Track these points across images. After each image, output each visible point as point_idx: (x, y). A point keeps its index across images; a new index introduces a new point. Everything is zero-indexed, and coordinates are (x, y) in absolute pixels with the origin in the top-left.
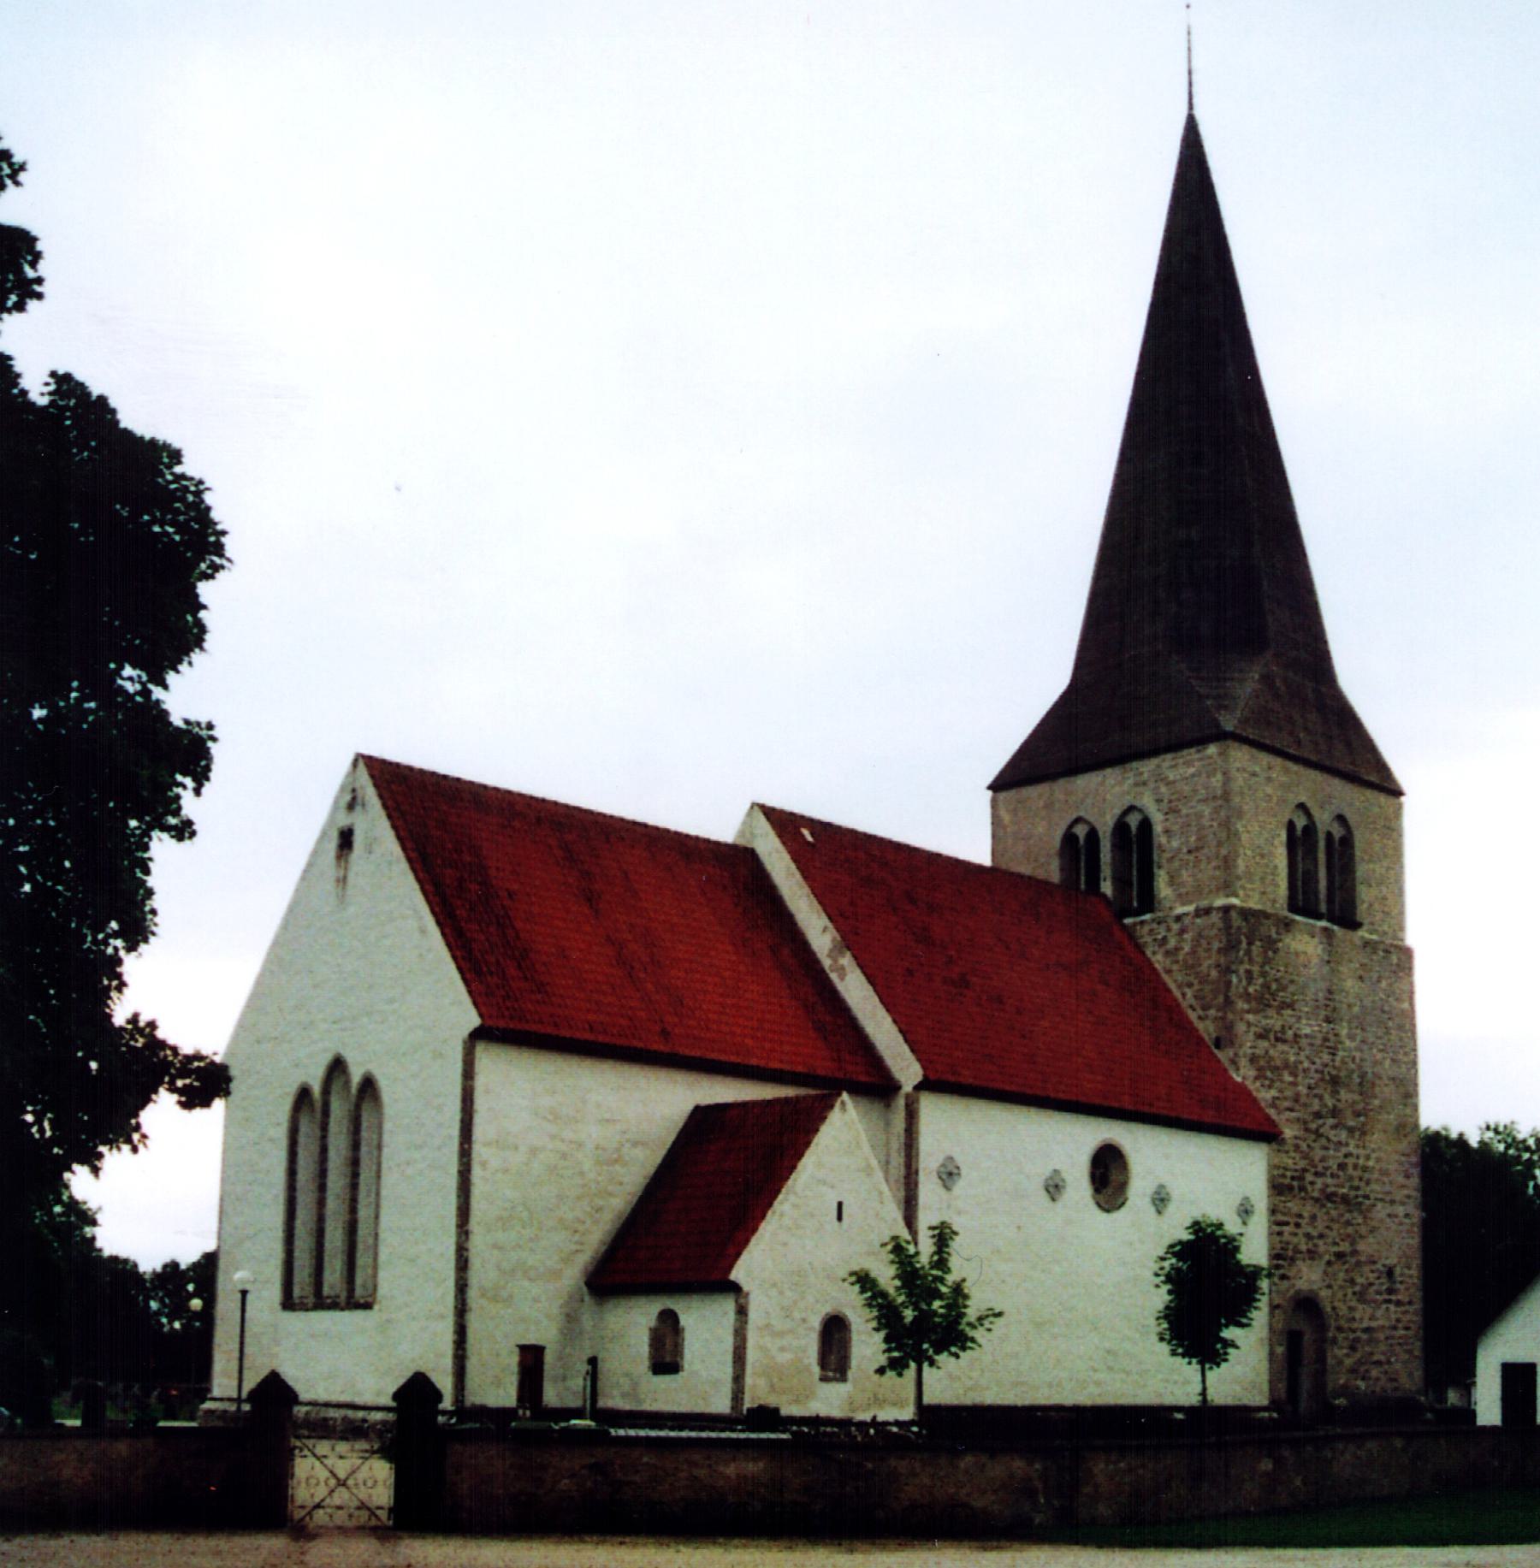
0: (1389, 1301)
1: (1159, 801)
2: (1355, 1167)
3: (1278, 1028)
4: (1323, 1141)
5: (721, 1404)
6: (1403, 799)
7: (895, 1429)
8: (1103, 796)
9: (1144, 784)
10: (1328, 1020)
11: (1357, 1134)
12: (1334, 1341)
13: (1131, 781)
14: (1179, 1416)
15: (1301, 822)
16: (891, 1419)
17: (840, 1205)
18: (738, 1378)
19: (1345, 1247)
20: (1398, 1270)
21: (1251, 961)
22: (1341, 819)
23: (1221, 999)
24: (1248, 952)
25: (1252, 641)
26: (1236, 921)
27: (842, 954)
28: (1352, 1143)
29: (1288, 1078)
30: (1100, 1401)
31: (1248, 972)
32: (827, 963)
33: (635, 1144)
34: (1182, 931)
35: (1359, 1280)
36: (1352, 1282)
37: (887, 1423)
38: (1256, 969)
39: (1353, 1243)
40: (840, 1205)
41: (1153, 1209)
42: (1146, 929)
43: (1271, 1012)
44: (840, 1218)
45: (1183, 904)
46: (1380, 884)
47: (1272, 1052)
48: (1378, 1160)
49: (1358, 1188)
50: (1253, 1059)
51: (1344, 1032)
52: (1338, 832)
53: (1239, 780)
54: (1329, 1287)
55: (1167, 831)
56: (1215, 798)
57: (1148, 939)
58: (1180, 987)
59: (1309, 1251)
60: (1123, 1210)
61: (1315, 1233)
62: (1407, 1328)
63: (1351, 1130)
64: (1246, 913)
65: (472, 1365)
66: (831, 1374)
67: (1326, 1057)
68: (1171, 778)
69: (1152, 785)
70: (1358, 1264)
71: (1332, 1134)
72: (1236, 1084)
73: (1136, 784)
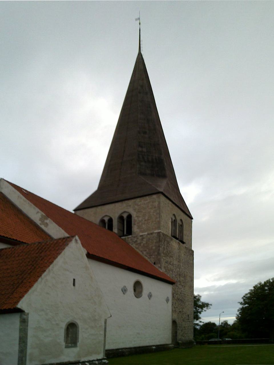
0: (188, 321)
2: (183, 293)
4: (177, 287)
6: (193, 220)
8: (114, 211)
10: (179, 262)
11: (183, 287)
12: (179, 329)
14: (154, 347)
15: (174, 218)
16: (95, 359)
17: (74, 280)
19: (181, 310)
20: (189, 316)
21: (164, 245)
22: (181, 220)
23: (156, 253)
25: (164, 176)
26: (162, 235)
28: (182, 288)
29: (171, 272)
30: (136, 346)
35: (183, 317)
36: (182, 317)
37: (93, 361)
38: (165, 247)
39: (182, 309)
40: (74, 280)
41: (148, 298)
42: (129, 239)
44: (74, 285)
47: (168, 266)
48: (187, 293)
49: (183, 298)
50: (165, 267)
51: (181, 265)
53: (162, 205)
55: (137, 217)
57: (131, 241)
59: (175, 310)
60: (141, 298)
61: (176, 307)
62: (191, 327)
63: (182, 286)
64: (163, 234)
66: (70, 345)
67: (178, 269)
68: (139, 204)
70: (183, 314)
71: (179, 286)
72: (161, 272)
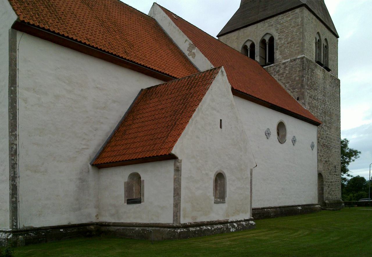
0: (335, 174)
1: (277, 30)
3: (314, 95)
5: (167, 219)
7: (244, 223)
8: (255, 34)
9: (272, 25)
10: (324, 96)
13: (267, 26)
15: (318, 38)
17: (221, 120)
18: (177, 205)
19: (327, 159)
20: (336, 167)
22: (326, 39)
24: (308, 72)
27: (193, 48)
31: (308, 78)
32: (187, 53)
33: (114, 102)
34: (285, 67)
38: (309, 77)
42: (272, 68)
43: (312, 90)
44: (221, 127)
45: (285, 59)
46: (333, 61)
52: (325, 44)
54: (324, 170)
56: (298, 25)
58: (284, 84)
61: (321, 155)
63: (328, 127)
65: (21, 207)
69: (274, 26)
73: (269, 26)
